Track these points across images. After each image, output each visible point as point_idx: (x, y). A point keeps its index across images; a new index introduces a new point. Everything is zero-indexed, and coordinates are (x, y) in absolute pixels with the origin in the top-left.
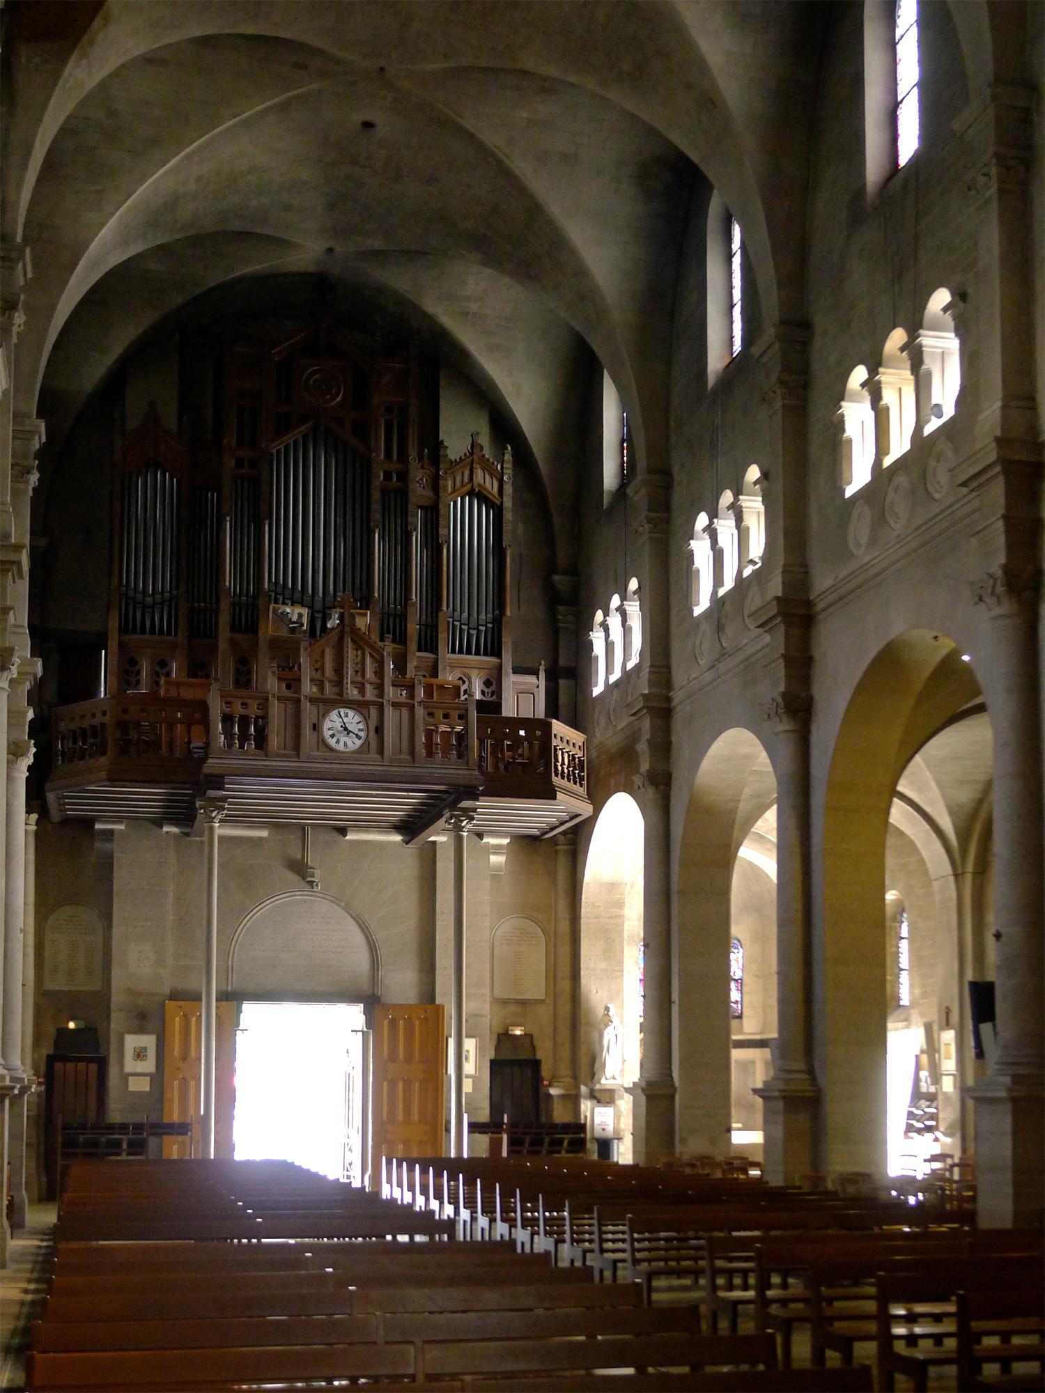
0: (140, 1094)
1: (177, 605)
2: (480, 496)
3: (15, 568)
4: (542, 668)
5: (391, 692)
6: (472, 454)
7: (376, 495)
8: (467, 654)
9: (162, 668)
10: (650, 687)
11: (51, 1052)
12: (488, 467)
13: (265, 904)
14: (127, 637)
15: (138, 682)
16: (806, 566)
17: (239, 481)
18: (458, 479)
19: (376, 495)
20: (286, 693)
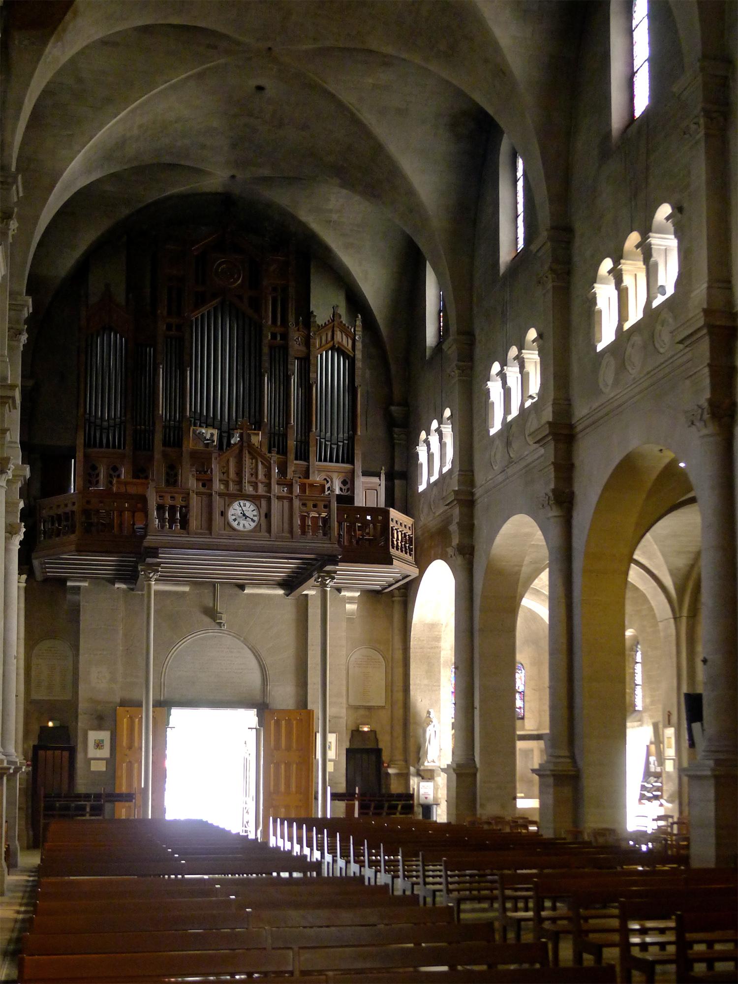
0: (99, 773)
1: (125, 427)
2: (339, 350)
3: (10, 401)
4: (383, 472)
5: (276, 489)
6: (333, 321)
7: (266, 350)
8: (330, 462)
9: (115, 472)
10: (459, 485)
11: (36, 743)
12: (344, 330)
13: (187, 638)
14: (90, 450)
15: (97, 482)
16: (569, 400)
17: (169, 340)
18: (324, 338)
19: (266, 350)
20: (202, 490)
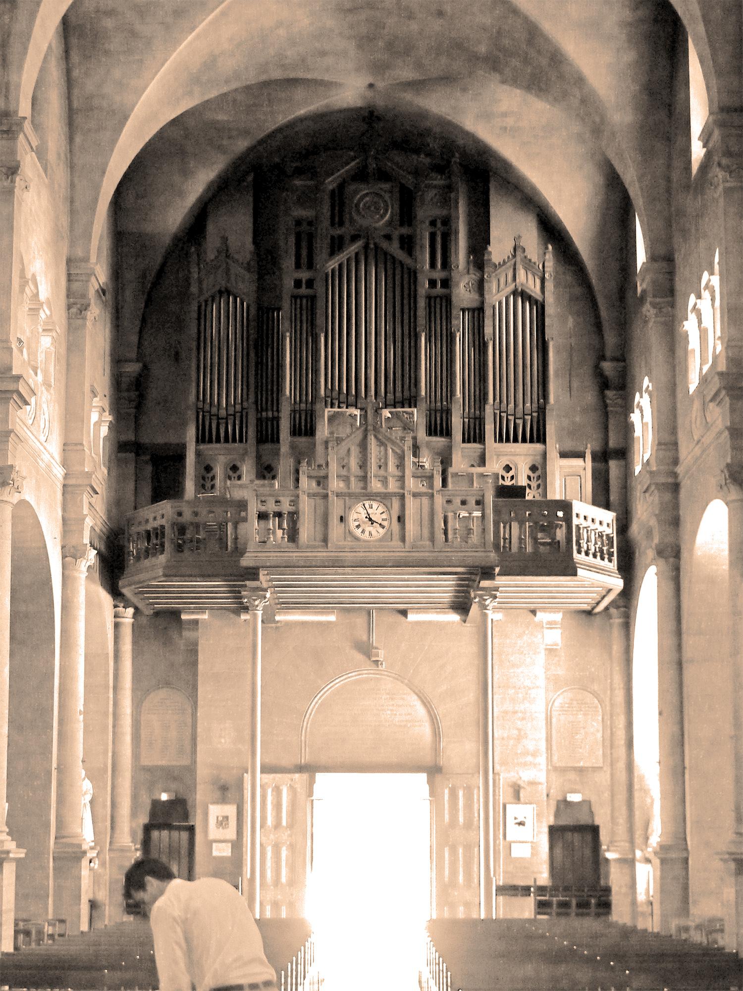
0: (222, 859)
3: (15, 396)
5: (411, 483)
6: (514, 256)
7: (422, 303)
10: (658, 465)
12: (529, 265)
13: (334, 682)
14: (202, 447)
15: (213, 487)
18: (502, 280)
19: (422, 303)
